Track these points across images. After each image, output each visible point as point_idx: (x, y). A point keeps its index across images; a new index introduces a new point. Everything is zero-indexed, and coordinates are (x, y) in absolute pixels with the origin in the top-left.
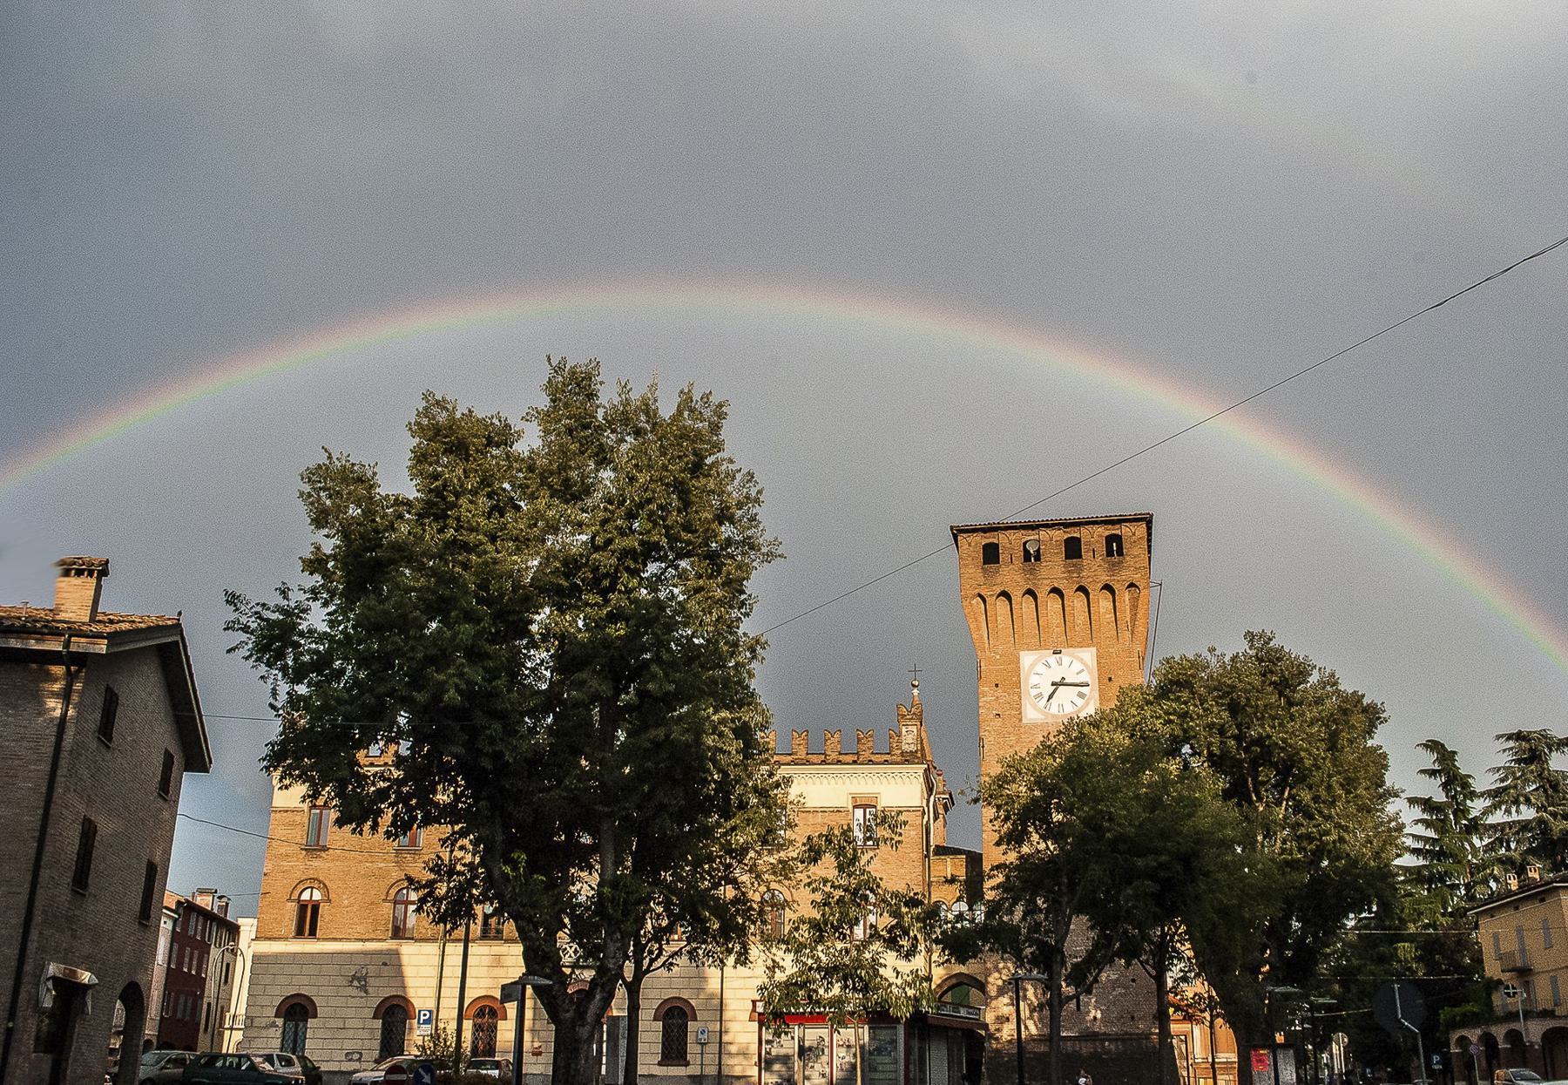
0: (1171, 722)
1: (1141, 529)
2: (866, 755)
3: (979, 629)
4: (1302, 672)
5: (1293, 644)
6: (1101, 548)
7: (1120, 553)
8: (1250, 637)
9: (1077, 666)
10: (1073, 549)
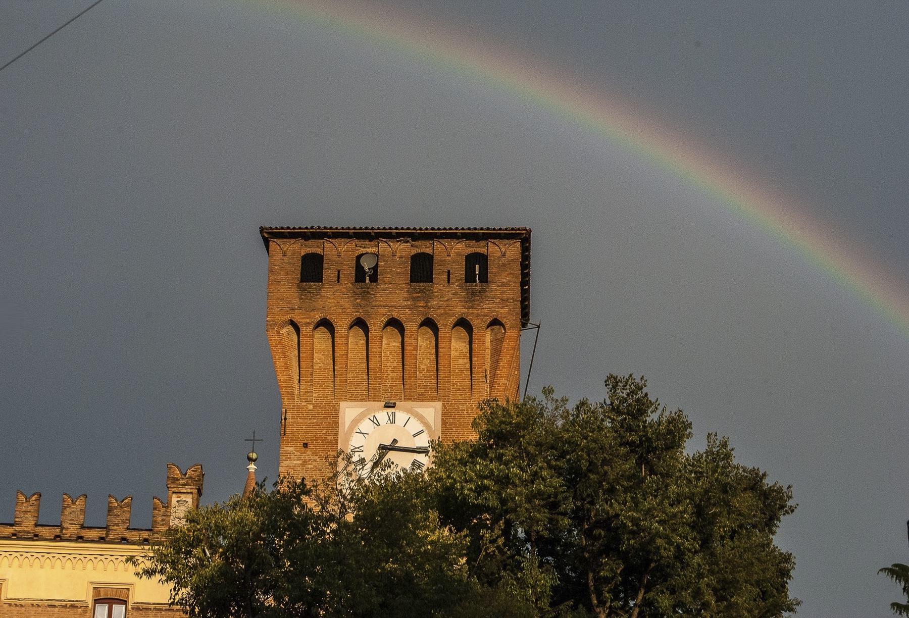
0: (486, 488)
1: (513, 250)
2: (118, 530)
3: (287, 367)
4: (675, 431)
5: (665, 401)
6: (459, 272)
7: (484, 279)
8: (613, 382)
9: (415, 425)
10: (422, 270)
